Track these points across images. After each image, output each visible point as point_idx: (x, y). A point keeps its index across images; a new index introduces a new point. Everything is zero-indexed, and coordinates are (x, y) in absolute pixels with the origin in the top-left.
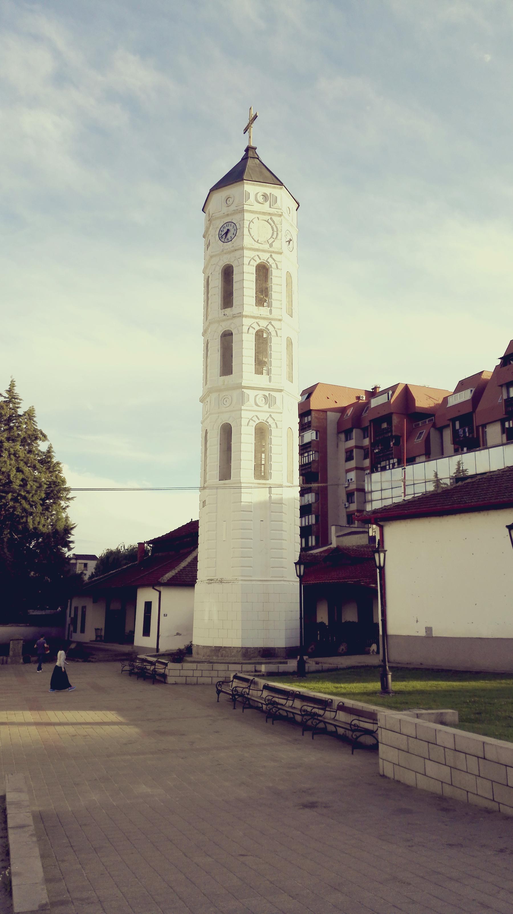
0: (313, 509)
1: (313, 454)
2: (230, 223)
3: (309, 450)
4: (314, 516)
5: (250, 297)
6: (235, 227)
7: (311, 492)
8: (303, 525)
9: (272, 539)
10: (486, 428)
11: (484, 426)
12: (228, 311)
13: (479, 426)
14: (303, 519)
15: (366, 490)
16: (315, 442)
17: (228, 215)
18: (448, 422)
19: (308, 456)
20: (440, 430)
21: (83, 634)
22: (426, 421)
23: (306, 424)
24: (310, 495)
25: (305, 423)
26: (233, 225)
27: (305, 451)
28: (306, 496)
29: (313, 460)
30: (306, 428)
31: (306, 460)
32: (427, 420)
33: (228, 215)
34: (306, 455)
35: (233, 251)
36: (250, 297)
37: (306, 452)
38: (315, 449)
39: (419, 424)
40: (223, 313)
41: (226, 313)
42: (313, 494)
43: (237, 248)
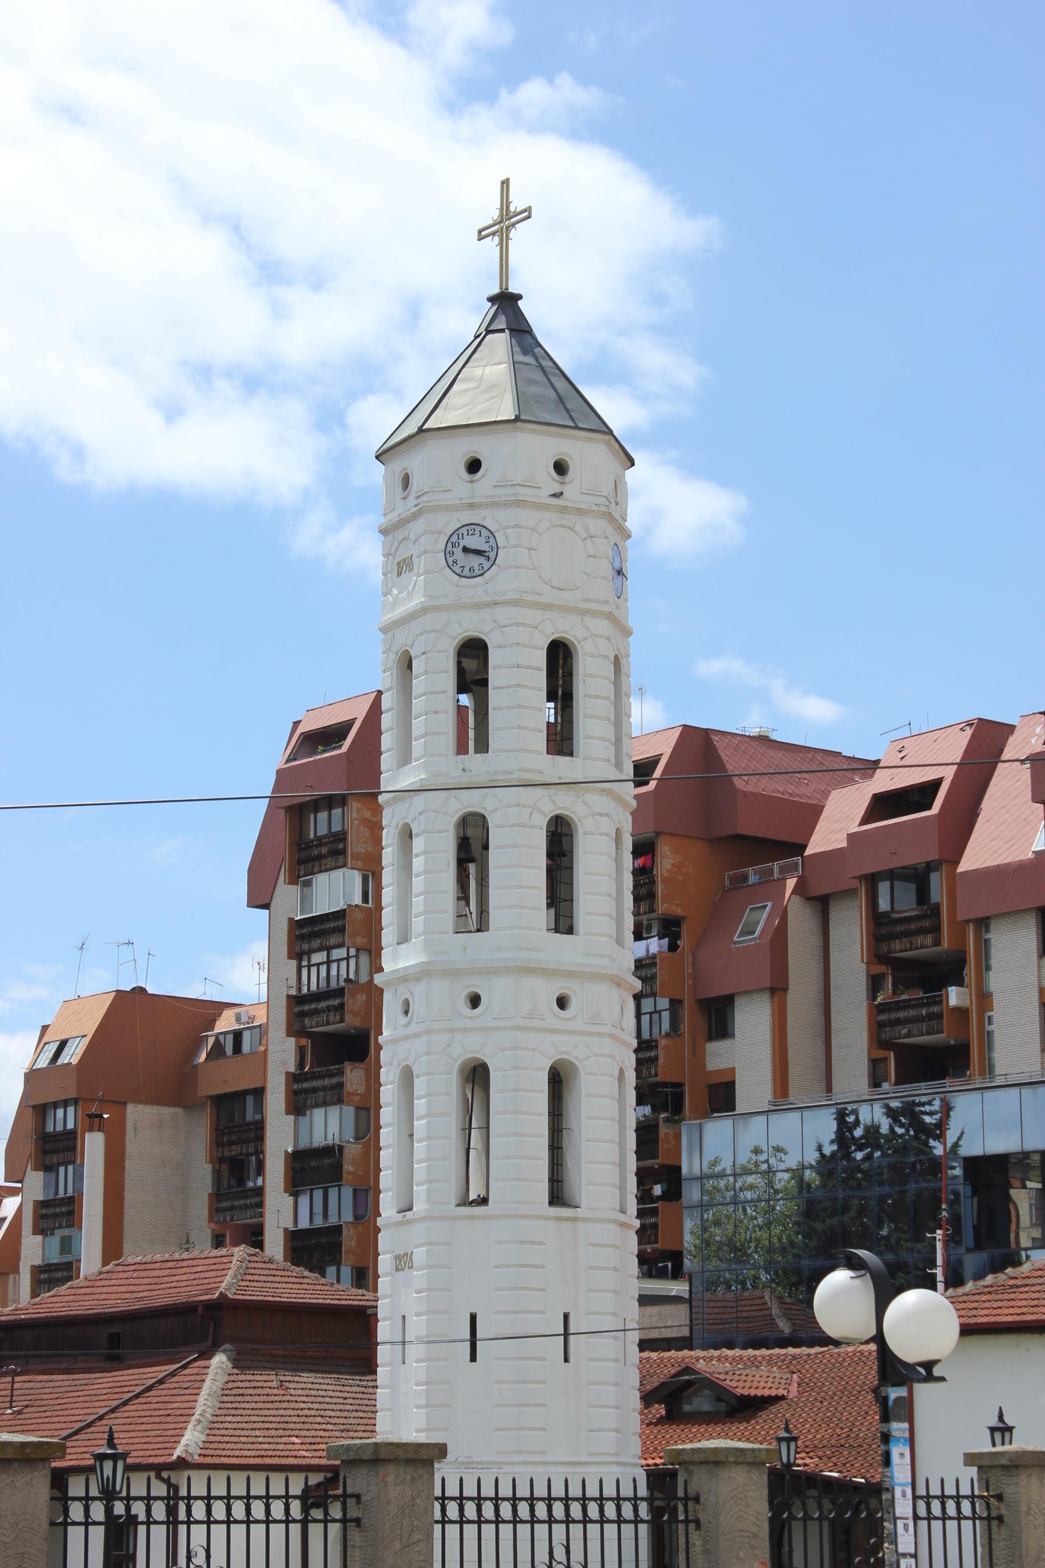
0: (348, 1167)
1: (348, 958)
2: (478, 528)
3: (333, 940)
4: (347, 1193)
5: (534, 688)
6: (492, 539)
7: (340, 1101)
8: (304, 1223)
9: (591, 1359)
10: (987, 931)
11: (983, 923)
12: (473, 759)
13: (968, 921)
14: (304, 1201)
15: (685, 1170)
16: (359, 915)
17: (471, 506)
18: (856, 883)
19: (329, 962)
20: (822, 904)
21: (961, 1459)
22: (772, 870)
23: (320, 841)
24: (334, 1112)
25: (319, 839)
26: (485, 533)
27: (316, 943)
28: (318, 1114)
29: (348, 980)
30: (320, 857)
31: (313, 981)
32: (776, 866)
33: (471, 506)
34: (318, 957)
35: (487, 605)
36: (534, 688)
37: (320, 949)
38: (360, 941)
39: (745, 878)
40: (461, 767)
41: (467, 765)
42: (349, 1111)
43: (498, 598)
